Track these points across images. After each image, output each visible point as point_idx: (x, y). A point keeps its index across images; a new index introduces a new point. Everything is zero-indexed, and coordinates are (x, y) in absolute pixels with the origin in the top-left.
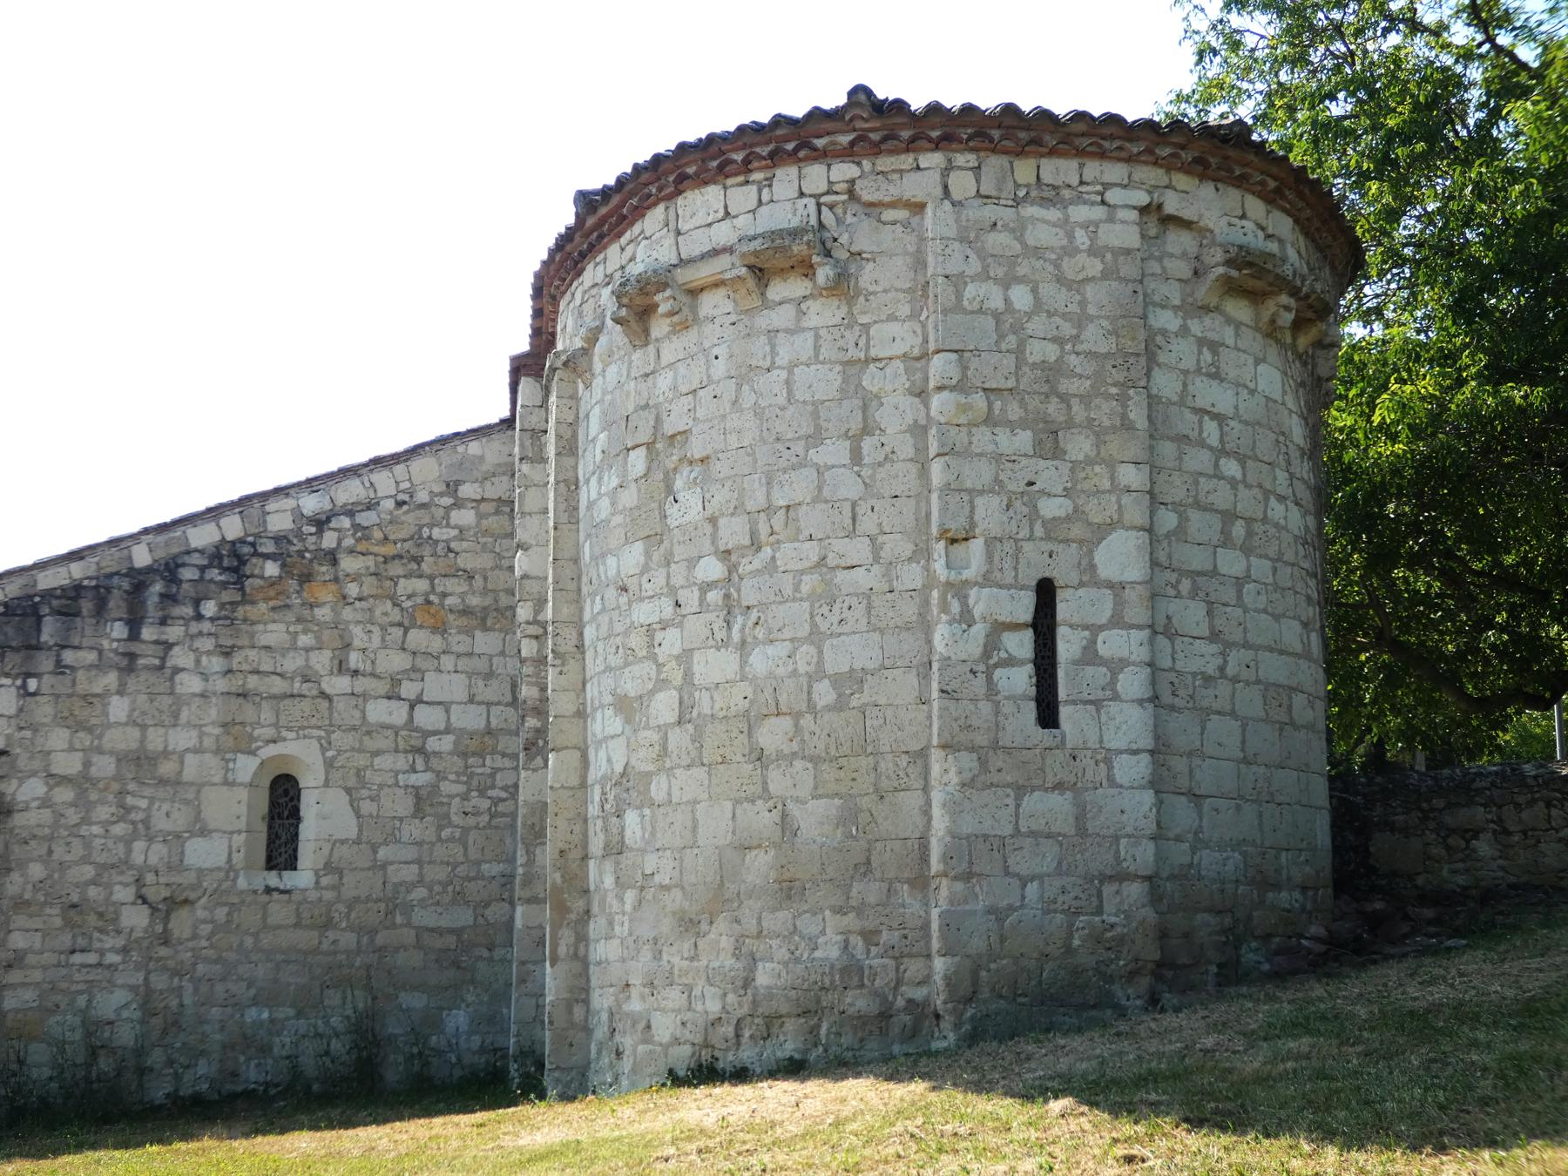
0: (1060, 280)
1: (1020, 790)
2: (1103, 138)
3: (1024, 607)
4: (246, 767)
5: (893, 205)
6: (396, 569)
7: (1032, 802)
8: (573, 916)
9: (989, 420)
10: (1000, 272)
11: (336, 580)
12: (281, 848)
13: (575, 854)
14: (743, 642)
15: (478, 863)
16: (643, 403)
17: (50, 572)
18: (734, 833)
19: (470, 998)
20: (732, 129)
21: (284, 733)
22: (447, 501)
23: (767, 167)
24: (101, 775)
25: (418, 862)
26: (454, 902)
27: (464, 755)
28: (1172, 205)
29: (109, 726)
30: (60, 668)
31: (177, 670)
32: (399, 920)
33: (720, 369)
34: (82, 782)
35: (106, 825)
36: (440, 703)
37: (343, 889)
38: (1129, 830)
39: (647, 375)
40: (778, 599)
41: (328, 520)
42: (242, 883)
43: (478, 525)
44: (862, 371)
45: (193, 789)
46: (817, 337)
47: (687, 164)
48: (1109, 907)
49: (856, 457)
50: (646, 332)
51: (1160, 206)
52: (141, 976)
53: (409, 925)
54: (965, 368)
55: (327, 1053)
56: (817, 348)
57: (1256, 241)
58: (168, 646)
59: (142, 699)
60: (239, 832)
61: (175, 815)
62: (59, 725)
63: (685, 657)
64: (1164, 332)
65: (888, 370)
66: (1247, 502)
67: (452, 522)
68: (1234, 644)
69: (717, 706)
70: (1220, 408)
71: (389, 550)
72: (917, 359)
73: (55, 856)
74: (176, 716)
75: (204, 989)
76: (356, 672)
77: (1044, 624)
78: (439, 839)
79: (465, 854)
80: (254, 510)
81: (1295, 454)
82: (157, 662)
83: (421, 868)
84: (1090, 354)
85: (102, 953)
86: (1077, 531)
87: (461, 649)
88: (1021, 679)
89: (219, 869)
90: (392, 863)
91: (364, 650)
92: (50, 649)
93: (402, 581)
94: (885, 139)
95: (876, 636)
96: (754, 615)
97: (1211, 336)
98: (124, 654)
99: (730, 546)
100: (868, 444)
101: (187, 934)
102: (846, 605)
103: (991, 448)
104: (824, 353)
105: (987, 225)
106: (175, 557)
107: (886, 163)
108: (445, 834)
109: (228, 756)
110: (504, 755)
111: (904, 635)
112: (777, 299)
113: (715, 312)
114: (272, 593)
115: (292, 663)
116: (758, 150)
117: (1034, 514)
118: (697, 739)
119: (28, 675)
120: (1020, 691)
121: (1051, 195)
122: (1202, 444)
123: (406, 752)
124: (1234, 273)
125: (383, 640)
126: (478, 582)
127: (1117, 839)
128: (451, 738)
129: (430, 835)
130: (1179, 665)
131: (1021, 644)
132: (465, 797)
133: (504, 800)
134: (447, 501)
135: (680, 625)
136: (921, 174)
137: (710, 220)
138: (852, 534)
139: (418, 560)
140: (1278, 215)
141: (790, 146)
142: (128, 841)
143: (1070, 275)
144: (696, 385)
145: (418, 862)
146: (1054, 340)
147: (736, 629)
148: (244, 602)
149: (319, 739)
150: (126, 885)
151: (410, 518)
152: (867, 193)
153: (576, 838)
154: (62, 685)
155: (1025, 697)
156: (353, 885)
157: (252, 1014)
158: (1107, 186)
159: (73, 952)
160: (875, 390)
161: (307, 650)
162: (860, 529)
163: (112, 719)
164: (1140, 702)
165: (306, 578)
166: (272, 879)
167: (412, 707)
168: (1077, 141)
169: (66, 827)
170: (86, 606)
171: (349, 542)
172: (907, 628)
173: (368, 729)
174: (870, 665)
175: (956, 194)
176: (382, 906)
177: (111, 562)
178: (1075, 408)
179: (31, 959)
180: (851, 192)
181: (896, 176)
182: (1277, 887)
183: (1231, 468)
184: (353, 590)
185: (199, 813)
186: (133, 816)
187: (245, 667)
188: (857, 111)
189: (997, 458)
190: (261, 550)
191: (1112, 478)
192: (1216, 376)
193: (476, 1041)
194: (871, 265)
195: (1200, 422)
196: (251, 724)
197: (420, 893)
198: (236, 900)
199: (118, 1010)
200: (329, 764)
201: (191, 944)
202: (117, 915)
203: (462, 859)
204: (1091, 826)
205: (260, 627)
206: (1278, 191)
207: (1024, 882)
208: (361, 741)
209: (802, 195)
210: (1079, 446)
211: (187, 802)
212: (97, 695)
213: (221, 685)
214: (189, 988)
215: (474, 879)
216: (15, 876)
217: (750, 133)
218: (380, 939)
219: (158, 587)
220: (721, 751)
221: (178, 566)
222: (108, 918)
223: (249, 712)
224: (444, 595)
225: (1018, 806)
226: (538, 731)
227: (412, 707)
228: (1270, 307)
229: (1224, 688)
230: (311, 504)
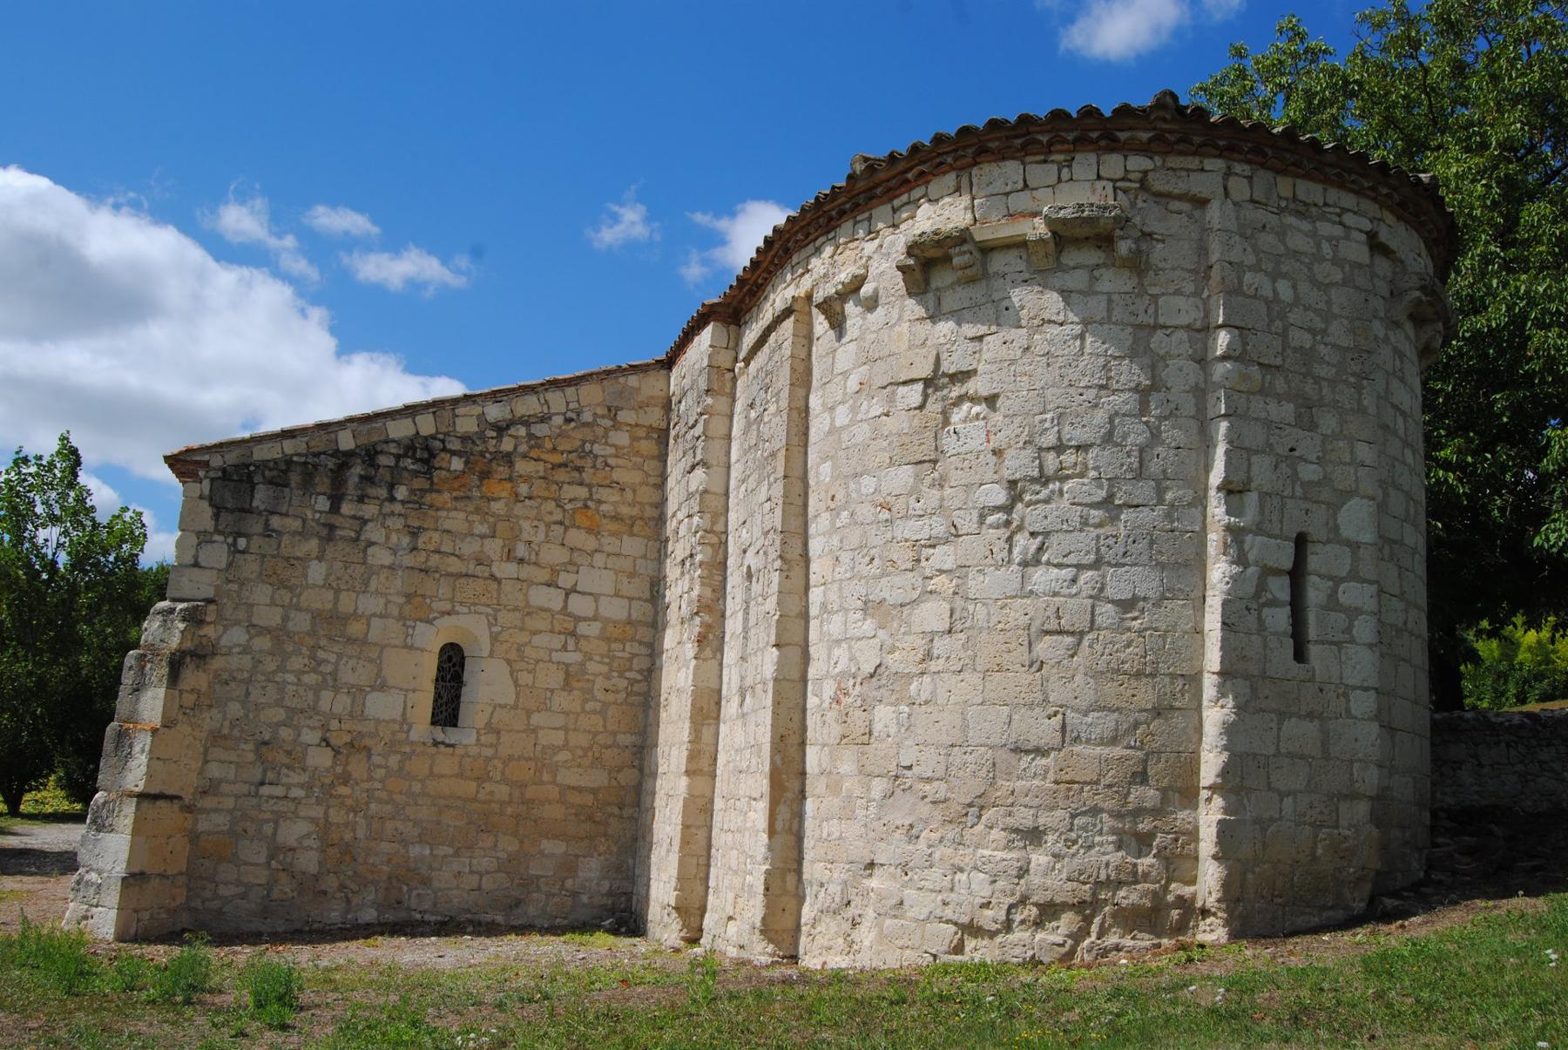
0: (1313, 281)
1: (1282, 716)
5: (1179, 198)
6: (561, 475)
7: (1290, 726)
8: (789, 795)
9: (1262, 391)
12: (447, 711)
15: (614, 734)
21: (458, 608)
23: (1069, 151)
25: (566, 729)
26: (592, 766)
27: (608, 640)
28: (1384, 236)
29: (308, 587)
30: (268, 532)
31: (370, 544)
34: (280, 634)
35: (299, 674)
41: (508, 427)
44: (1151, 335)
46: (1110, 301)
47: (990, 140)
48: (1343, 823)
49: (1144, 409)
50: (927, 282)
53: (554, 782)
54: (1245, 344)
55: (479, 889)
56: (1109, 310)
58: (364, 522)
59: (338, 565)
65: (1174, 338)
71: (557, 459)
72: (1198, 331)
73: (252, 698)
74: (366, 583)
76: (521, 561)
77: (1297, 575)
78: (583, 711)
80: (447, 414)
82: (353, 534)
84: (1334, 346)
85: (288, 787)
86: (1326, 495)
88: (1280, 618)
89: (394, 721)
90: (542, 728)
91: (530, 543)
92: (260, 513)
93: (565, 487)
94: (1179, 141)
98: (324, 525)
103: (1263, 415)
104: (1117, 314)
105: (1259, 226)
106: (374, 445)
107: (1175, 161)
108: (589, 706)
112: (1071, 264)
113: (1006, 269)
114: (456, 485)
115: (469, 547)
117: (1294, 477)
119: (240, 535)
121: (1302, 210)
122: (1395, 434)
126: (629, 494)
127: (1351, 762)
131: (1280, 588)
133: (638, 681)
136: (1206, 177)
137: (1008, 189)
141: (1094, 135)
142: (317, 690)
143: (1320, 278)
145: (566, 729)
148: (431, 491)
149: (488, 615)
151: (578, 435)
152: (1158, 183)
157: (415, 851)
158: (1344, 210)
159: (262, 784)
160: (1162, 353)
161: (483, 537)
163: (310, 581)
164: (1370, 646)
165: (485, 475)
167: (567, 595)
168: (1328, 170)
170: (295, 478)
171: (523, 448)
173: (530, 611)
175: (1235, 196)
176: (532, 764)
177: (319, 443)
178: (1325, 391)
179: (225, 788)
180: (1143, 181)
181: (1184, 173)
184: (523, 489)
185: (380, 670)
186: (322, 668)
188: (1161, 113)
189: (1268, 423)
190: (449, 446)
191: (1352, 453)
193: (606, 886)
194: (1160, 246)
197: (563, 756)
198: (407, 749)
199: (300, 840)
200: (494, 639)
202: (305, 754)
205: (443, 513)
207: (1283, 795)
209: (1099, 177)
210: (1328, 422)
211: (371, 661)
212: (298, 558)
219: (357, 470)
220: (998, 660)
221: (377, 453)
222: (296, 758)
224: (600, 502)
227: (567, 595)
230: (494, 412)
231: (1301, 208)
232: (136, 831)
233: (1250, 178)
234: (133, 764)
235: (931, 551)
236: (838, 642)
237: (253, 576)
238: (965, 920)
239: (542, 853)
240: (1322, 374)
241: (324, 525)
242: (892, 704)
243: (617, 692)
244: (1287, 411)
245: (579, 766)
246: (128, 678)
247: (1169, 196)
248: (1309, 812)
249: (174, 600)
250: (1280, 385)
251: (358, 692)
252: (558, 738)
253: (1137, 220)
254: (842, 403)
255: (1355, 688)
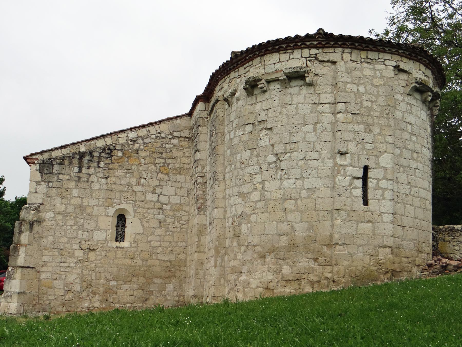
1: (358, 222)
2: (386, 47)
3: (360, 173)
4: (111, 211)
5: (328, 61)
6: (156, 155)
7: (361, 225)
8: (221, 254)
10: (356, 82)
11: (138, 158)
13: (222, 237)
14: (281, 179)
15: (177, 242)
16: (251, 112)
17: (56, 152)
18: (277, 231)
19: (174, 281)
20: (283, 38)
22: (170, 137)
24: (70, 212)
25: (160, 241)
26: (169, 253)
28: (402, 66)
30: (59, 180)
31: (92, 182)
32: (154, 257)
33: (276, 104)
34: (64, 214)
36: (167, 195)
37: (138, 248)
38: (386, 234)
39: (252, 104)
40: (292, 167)
42: (109, 245)
43: (179, 144)
45: (96, 217)
46: (305, 96)
49: (315, 130)
51: (399, 66)
52: (80, 270)
56: (305, 99)
57: (423, 77)
58: (90, 175)
59: (82, 190)
60: (109, 230)
61: (91, 224)
62: (58, 197)
63: (262, 183)
64: (398, 100)
66: (417, 149)
67: (171, 143)
68: (413, 186)
69: (273, 196)
70: (412, 122)
73: (56, 235)
74: (92, 195)
75: (98, 275)
77: (365, 178)
79: (173, 239)
81: (429, 135)
83: (160, 243)
84: (380, 105)
87: (173, 180)
88: (359, 192)
89: (103, 240)
90: (152, 241)
95: (319, 179)
96: (284, 171)
97: (410, 102)
98: (77, 177)
99: (278, 152)
100: (318, 126)
101: (94, 259)
102: (311, 170)
105: (353, 69)
107: (326, 50)
108: (168, 233)
109: (106, 208)
110: (185, 211)
111: (327, 179)
112: (293, 85)
114: (120, 161)
116: (290, 44)
118: (266, 205)
119: (50, 182)
120: (358, 195)
122: (407, 131)
123: (157, 209)
124: (418, 86)
125: (151, 176)
127: (383, 236)
128: (170, 205)
129: (163, 233)
130: (399, 191)
131: (359, 183)
132: (173, 223)
134: (170, 137)
135: (261, 174)
137: (274, 62)
138: (313, 150)
139: (162, 153)
140: (428, 70)
144: (268, 107)
146: (370, 101)
147: (279, 175)
148: (112, 163)
150: (76, 244)
153: (222, 233)
154: (59, 185)
155: (360, 196)
156: (141, 247)
157: (112, 283)
162: (315, 150)
164: (390, 200)
166: (118, 244)
167: (159, 196)
169: (60, 226)
170: (67, 162)
171: (142, 147)
172: (328, 177)
174: (317, 187)
175: (345, 60)
176: (149, 253)
179: (49, 264)
181: (328, 54)
182: (421, 252)
183: (414, 138)
184: (143, 161)
187: (111, 182)
189: (354, 132)
191: (385, 139)
192: (411, 113)
194: (321, 78)
195: (407, 125)
196: (113, 199)
200: (135, 211)
201: (95, 262)
203: (172, 241)
204: (377, 232)
205: (116, 171)
206: (428, 64)
208: (144, 205)
210: (376, 130)
213: (105, 187)
214: (94, 274)
215: (176, 246)
216: (45, 240)
217: (288, 39)
218: (149, 263)
219: (87, 158)
220: (273, 209)
222: (72, 254)
223: (112, 195)
224: (169, 164)
225: (357, 226)
226: (202, 204)
227: (159, 196)
228: (425, 95)
229: (410, 197)
230: (132, 135)
231: (369, 61)
232: (22, 278)
233: (351, 53)
234: (19, 257)
235: (255, 176)
236: (232, 206)
237: (54, 195)
238: (265, 287)
239: (154, 283)
240: (375, 115)
241: (77, 177)
242: (246, 224)
243: (177, 228)
244: (361, 128)
245: (165, 253)
246: (16, 230)
247: (324, 61)
248: (368, 251)
249: (29, 204)
250: (359, 119)
251: (90, 231)
252: (158, 244)
253: (313, 70)
254: (232, 131)
255: (384, 213)
